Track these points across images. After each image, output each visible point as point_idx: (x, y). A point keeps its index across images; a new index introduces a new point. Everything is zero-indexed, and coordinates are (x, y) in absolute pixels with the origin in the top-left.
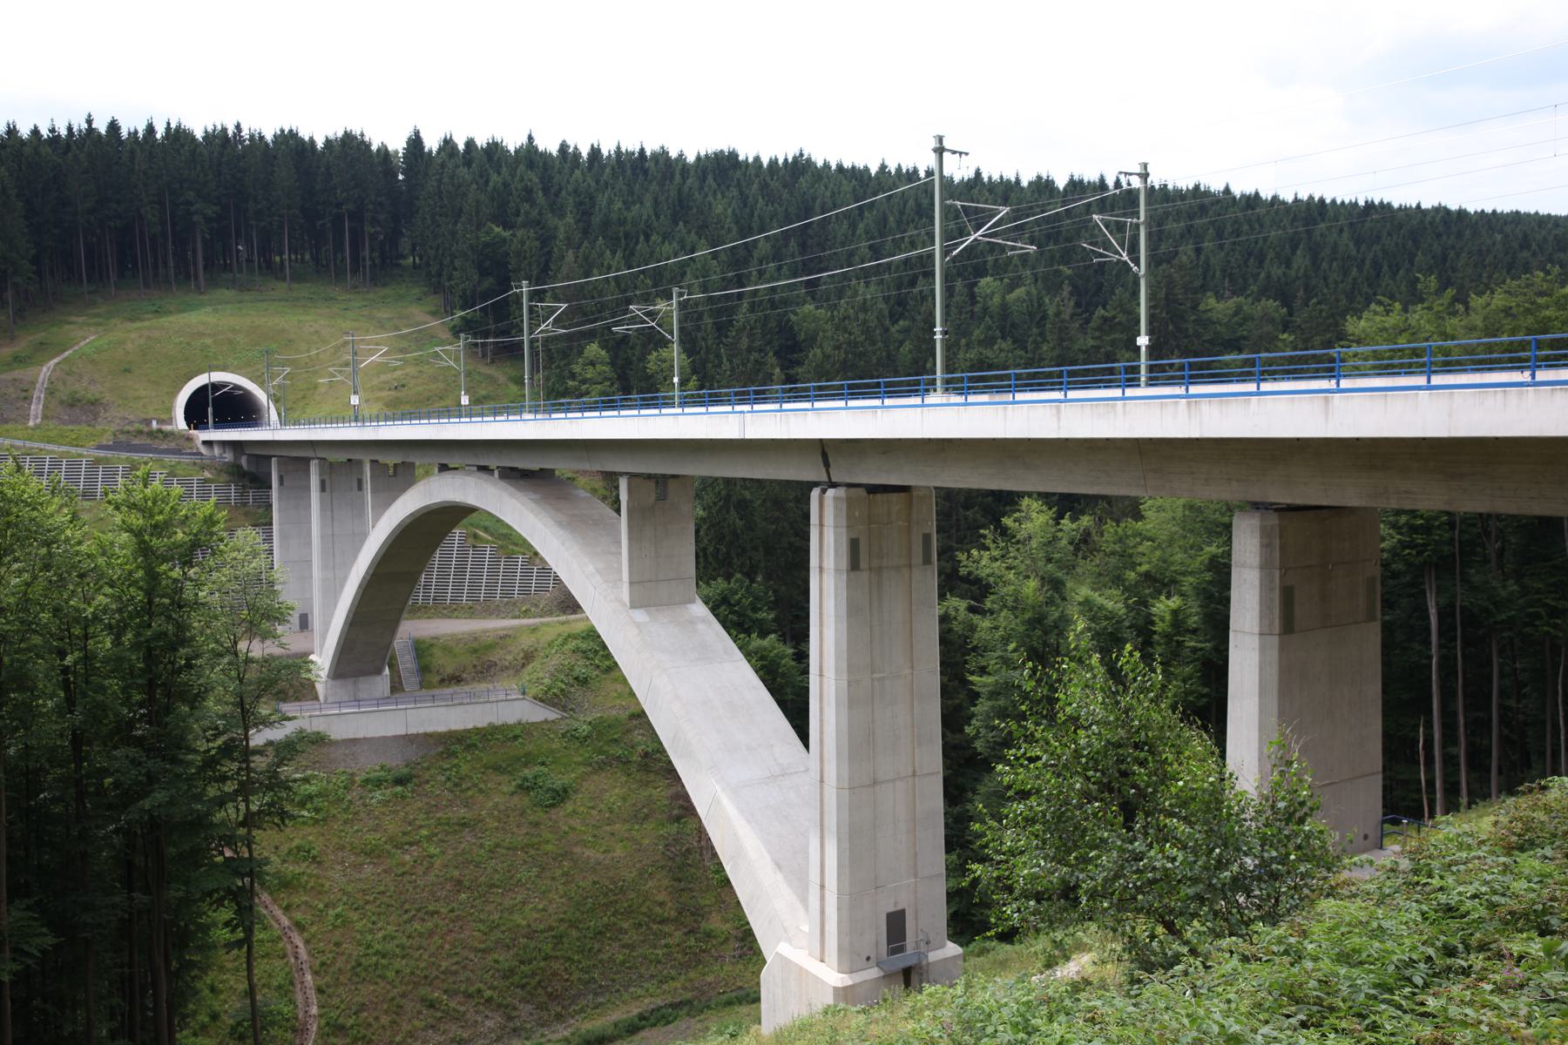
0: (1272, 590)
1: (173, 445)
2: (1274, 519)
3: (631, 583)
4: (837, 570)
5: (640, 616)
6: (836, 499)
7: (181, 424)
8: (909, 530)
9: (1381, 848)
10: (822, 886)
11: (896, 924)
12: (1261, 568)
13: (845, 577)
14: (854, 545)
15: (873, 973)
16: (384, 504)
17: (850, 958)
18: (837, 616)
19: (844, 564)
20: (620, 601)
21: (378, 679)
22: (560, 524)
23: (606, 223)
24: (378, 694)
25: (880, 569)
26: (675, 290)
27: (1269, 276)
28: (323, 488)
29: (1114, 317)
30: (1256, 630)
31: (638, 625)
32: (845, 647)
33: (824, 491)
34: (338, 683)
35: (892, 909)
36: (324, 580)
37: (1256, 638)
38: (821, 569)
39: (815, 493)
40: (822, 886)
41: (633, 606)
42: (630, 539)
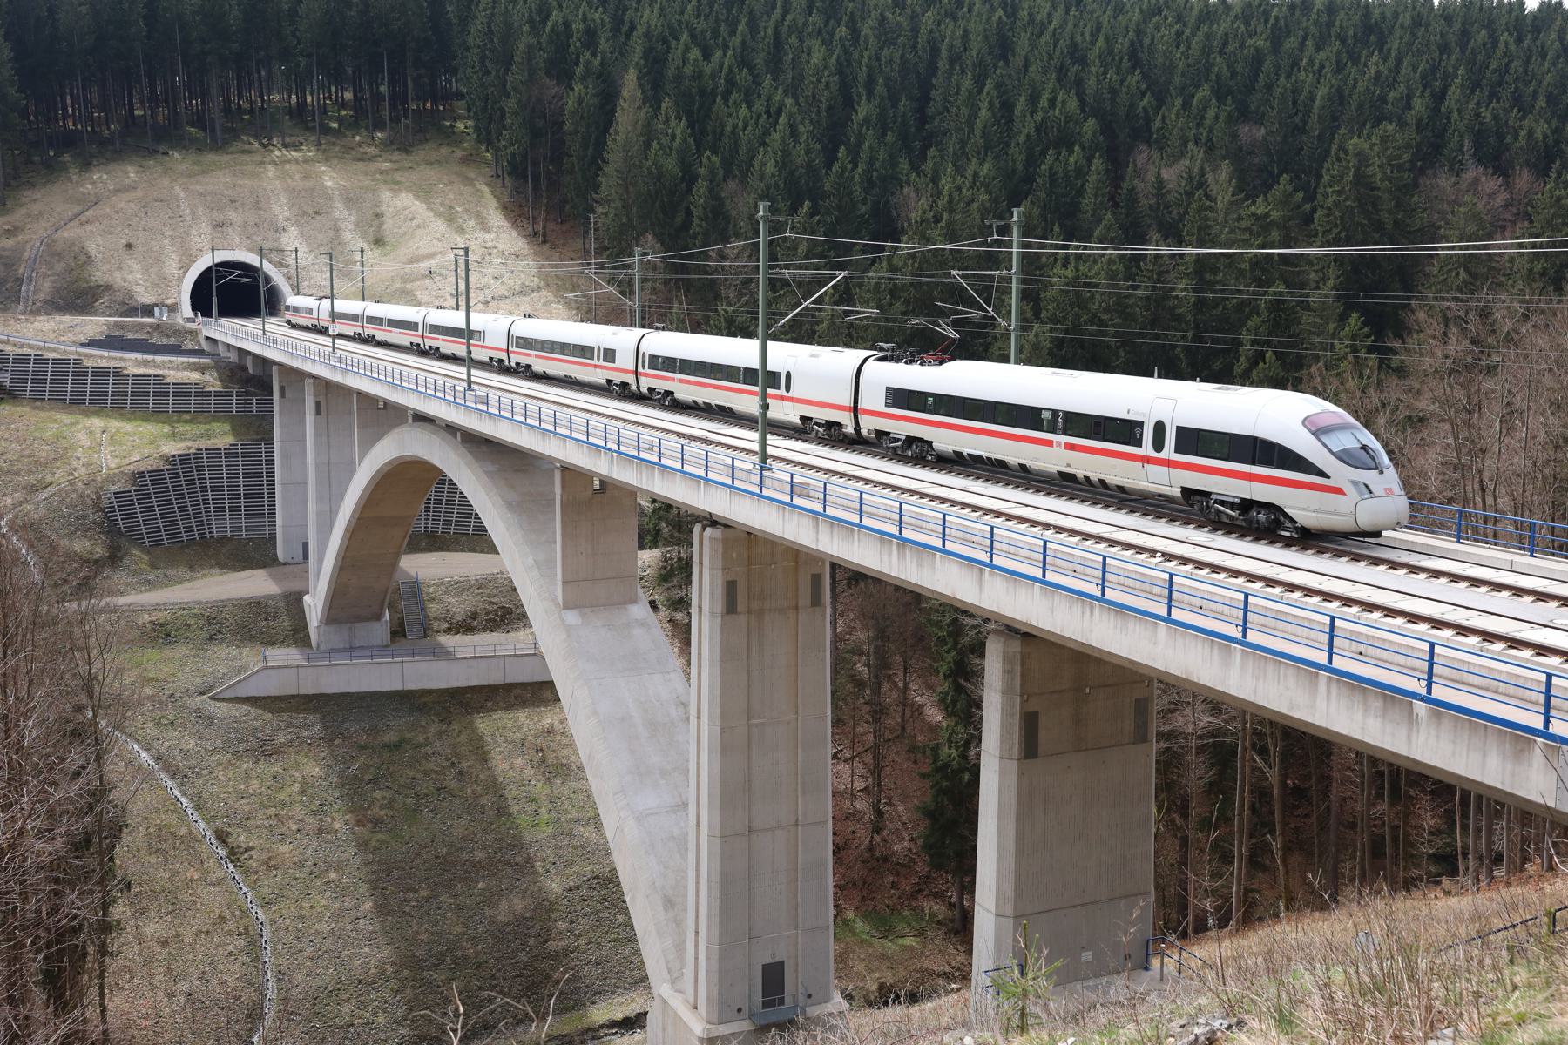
0: (1012, 715)
1: (172, 341)
2: (1016, 646)
3: (564, 582)
4: (712, 613)
5: (572, 617)
6: (712, 539)
7: (187, 310)
8: (796, 569)
9: (1147, 969)
10: (697, 933)
11: (773, 977)
12: (1004, 693)
13: (719, 620)
14: (731, 589)
15: (744, 1026)
16: (368, 444)
17: (724, 1009)
18: (711, 661)
19: (719, 607)
20: (554, 600)
21: (376, 625)
22: (509, 505)
23: (679, 77)
24: (377, 641)
25: (761, 613)
26: (637, 249)
27: (1530, 133)
28: (318, 412)
29: (1267, 215)
30: (997, 753)
31: (568, 629)
32: (718, 692)
33: (704, 528)
34: (331, 628)
35: (768, 960)
36: (319, 514)
37: (997, 761)
38: (700, 607)
39: (697, 528)
40: (697, 933)
41: (566, 607)
42: (563, 535)
